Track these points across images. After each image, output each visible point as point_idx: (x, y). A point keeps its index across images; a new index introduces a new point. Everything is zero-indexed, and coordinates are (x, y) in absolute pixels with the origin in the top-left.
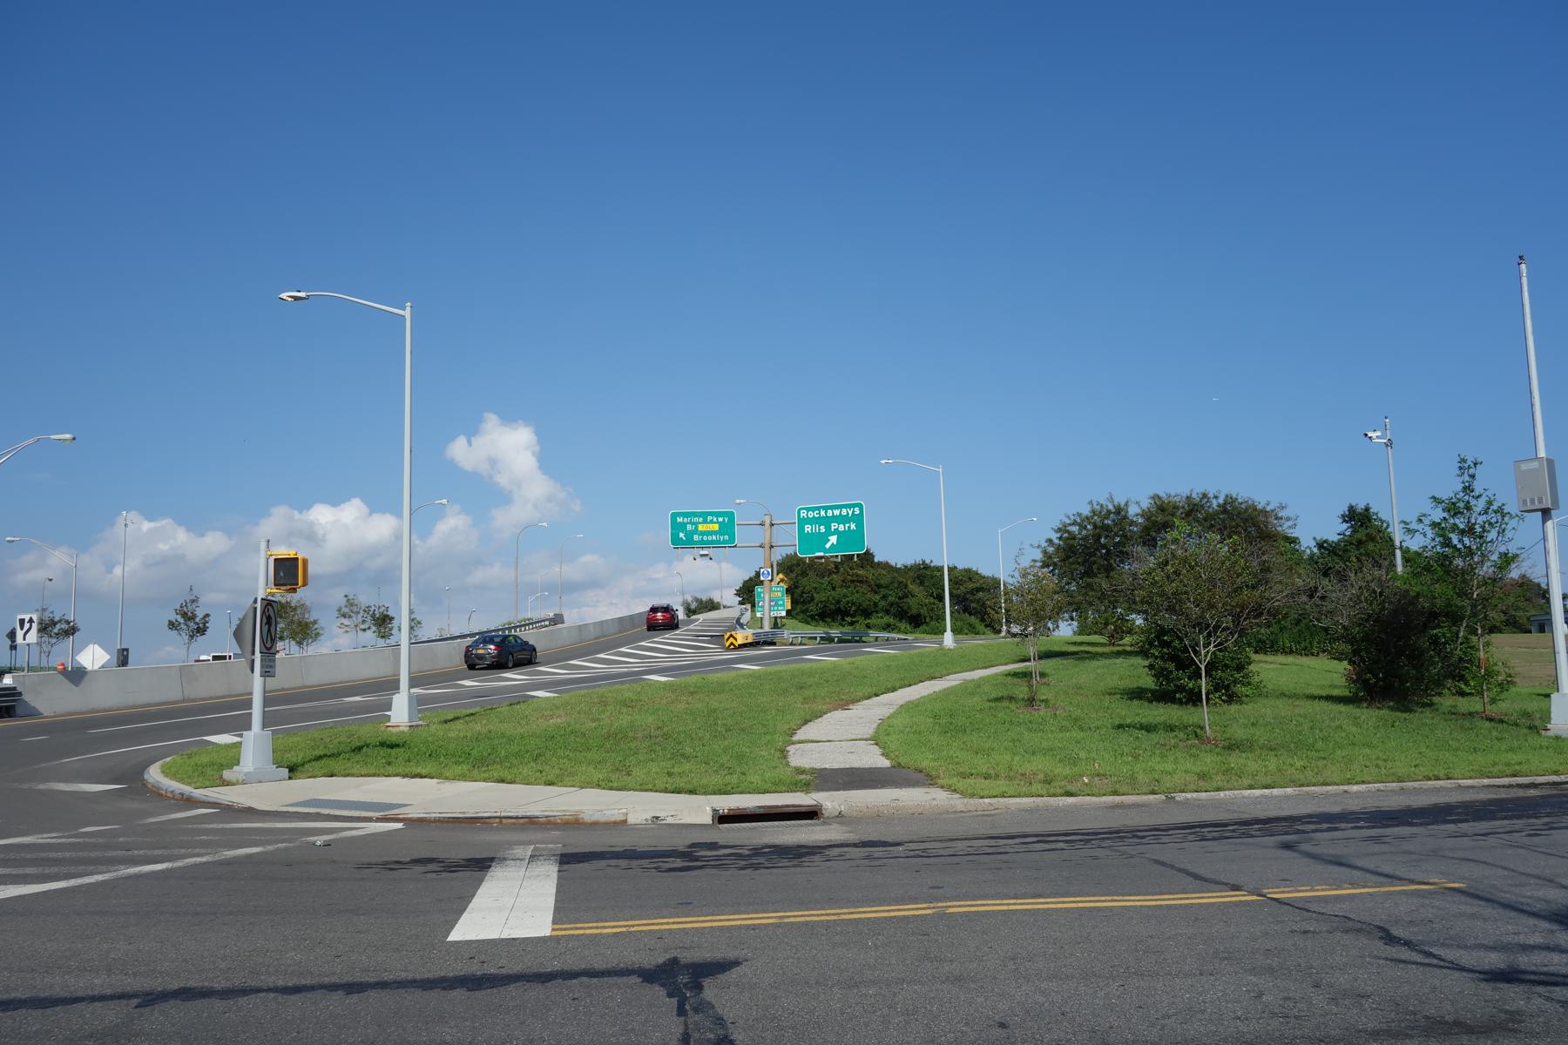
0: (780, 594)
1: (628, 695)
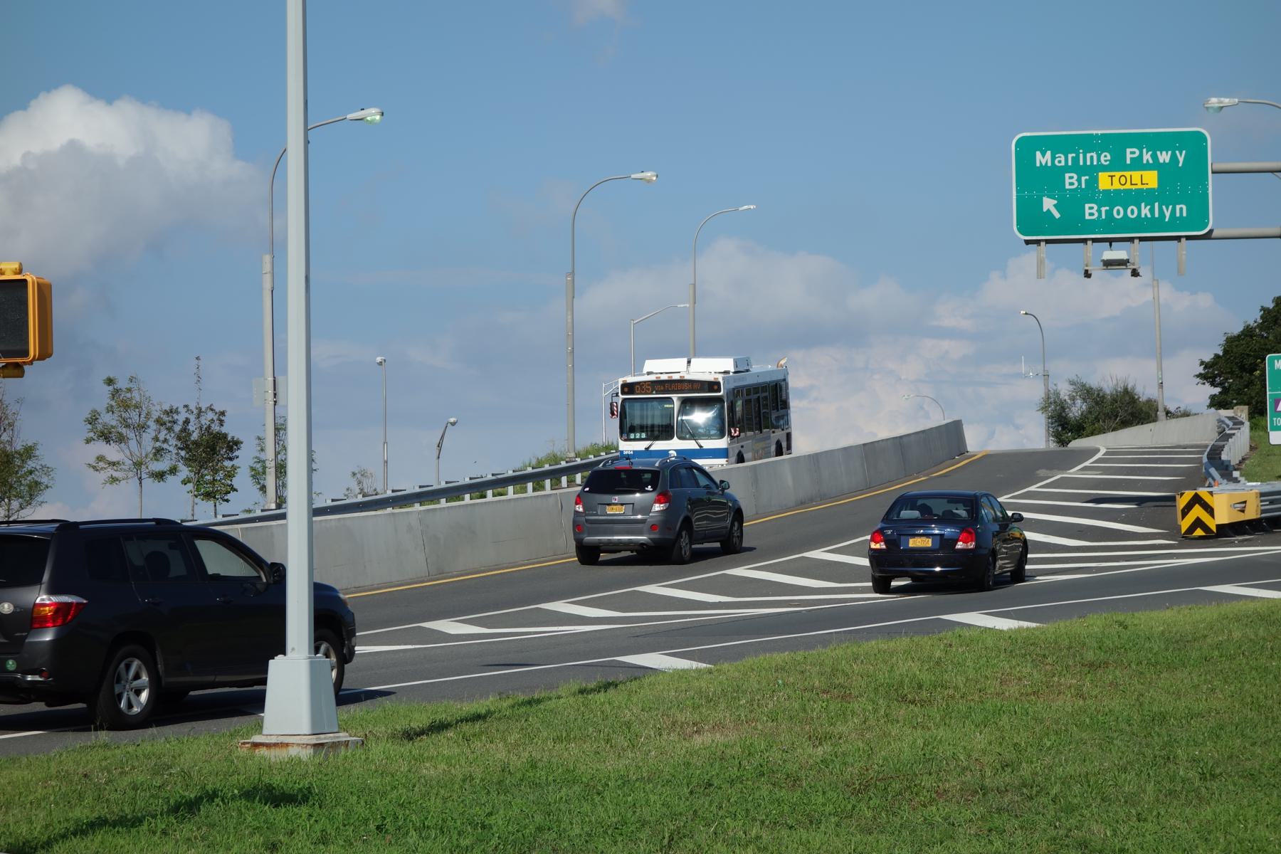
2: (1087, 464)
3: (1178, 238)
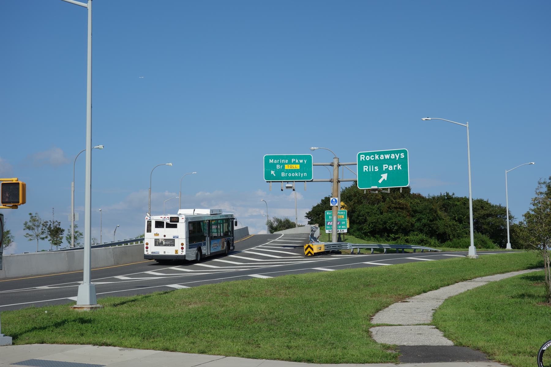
0: (343, 217)
1: (241, 288)
2: (280, 238)
3: (304, 181)
